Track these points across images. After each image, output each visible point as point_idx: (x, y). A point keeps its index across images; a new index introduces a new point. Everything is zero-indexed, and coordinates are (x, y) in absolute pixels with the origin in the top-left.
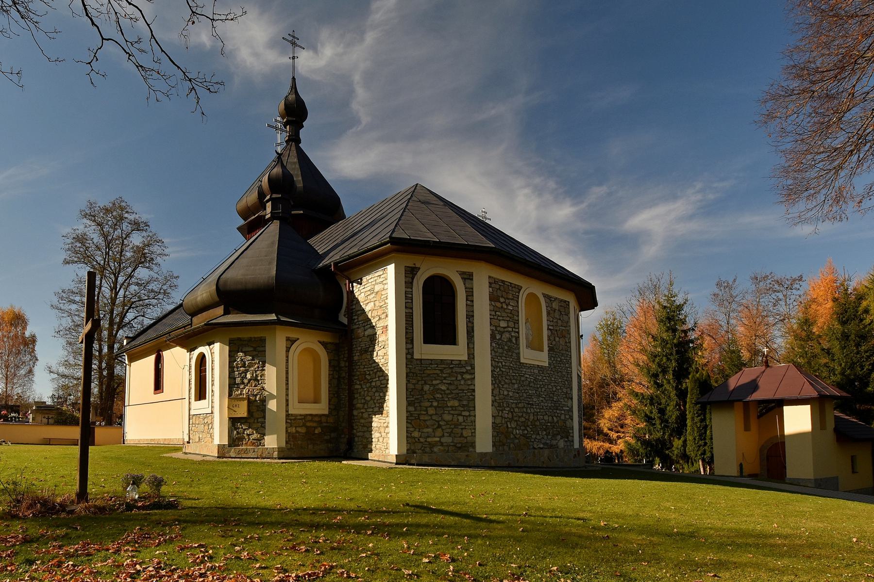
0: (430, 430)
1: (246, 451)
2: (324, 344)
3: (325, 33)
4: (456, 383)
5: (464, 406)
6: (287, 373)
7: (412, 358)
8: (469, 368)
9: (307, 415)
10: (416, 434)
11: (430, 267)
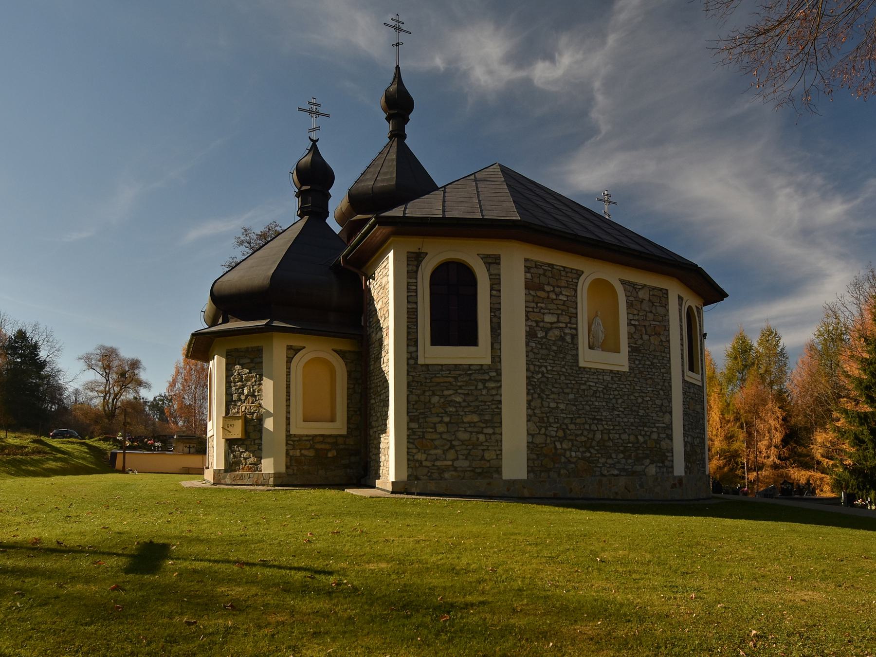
0: (439, 451)
1: (241, 477)
2: (341, 354)
3: (564, 40)
4: (475, 393)
5: (486, 421)
6: (288, 387)
7: (416, 363)
8: (494, 374)
9: (316, 436)
10: (420, 456)
11: (438, 252)
